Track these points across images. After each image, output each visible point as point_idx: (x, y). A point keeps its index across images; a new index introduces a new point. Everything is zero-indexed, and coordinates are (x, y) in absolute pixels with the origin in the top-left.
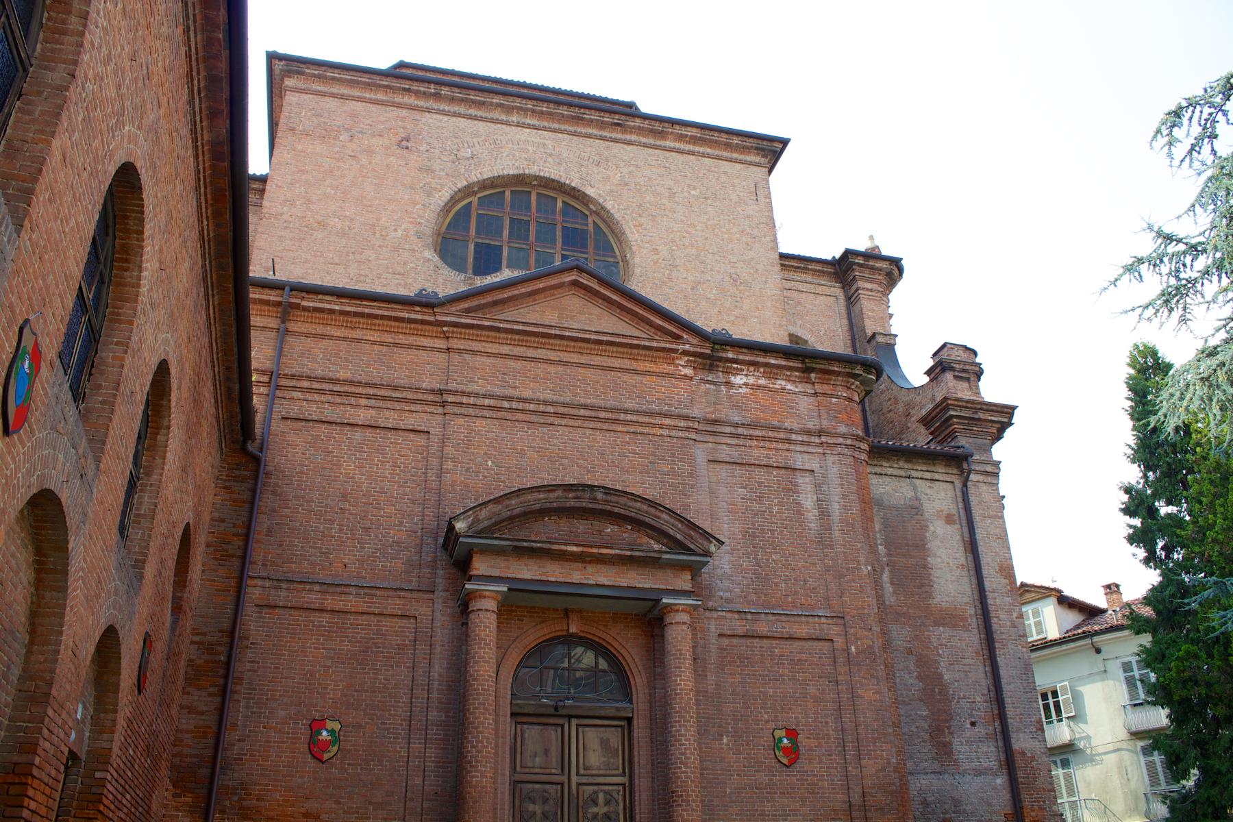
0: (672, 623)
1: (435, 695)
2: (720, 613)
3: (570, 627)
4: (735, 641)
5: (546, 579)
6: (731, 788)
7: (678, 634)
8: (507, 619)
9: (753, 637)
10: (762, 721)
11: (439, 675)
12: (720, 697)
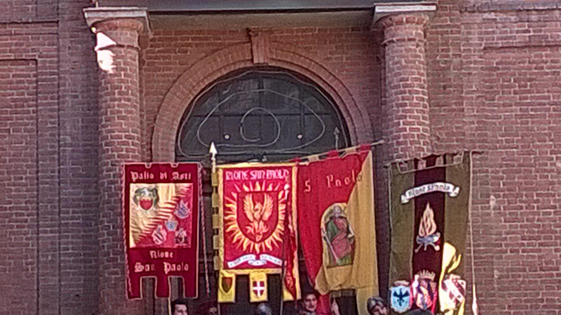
2: (486, 15)
3: (255, 54)
4: (511, 55)
9: (540, 47)
10: (552, 171)
12: (485, 141)
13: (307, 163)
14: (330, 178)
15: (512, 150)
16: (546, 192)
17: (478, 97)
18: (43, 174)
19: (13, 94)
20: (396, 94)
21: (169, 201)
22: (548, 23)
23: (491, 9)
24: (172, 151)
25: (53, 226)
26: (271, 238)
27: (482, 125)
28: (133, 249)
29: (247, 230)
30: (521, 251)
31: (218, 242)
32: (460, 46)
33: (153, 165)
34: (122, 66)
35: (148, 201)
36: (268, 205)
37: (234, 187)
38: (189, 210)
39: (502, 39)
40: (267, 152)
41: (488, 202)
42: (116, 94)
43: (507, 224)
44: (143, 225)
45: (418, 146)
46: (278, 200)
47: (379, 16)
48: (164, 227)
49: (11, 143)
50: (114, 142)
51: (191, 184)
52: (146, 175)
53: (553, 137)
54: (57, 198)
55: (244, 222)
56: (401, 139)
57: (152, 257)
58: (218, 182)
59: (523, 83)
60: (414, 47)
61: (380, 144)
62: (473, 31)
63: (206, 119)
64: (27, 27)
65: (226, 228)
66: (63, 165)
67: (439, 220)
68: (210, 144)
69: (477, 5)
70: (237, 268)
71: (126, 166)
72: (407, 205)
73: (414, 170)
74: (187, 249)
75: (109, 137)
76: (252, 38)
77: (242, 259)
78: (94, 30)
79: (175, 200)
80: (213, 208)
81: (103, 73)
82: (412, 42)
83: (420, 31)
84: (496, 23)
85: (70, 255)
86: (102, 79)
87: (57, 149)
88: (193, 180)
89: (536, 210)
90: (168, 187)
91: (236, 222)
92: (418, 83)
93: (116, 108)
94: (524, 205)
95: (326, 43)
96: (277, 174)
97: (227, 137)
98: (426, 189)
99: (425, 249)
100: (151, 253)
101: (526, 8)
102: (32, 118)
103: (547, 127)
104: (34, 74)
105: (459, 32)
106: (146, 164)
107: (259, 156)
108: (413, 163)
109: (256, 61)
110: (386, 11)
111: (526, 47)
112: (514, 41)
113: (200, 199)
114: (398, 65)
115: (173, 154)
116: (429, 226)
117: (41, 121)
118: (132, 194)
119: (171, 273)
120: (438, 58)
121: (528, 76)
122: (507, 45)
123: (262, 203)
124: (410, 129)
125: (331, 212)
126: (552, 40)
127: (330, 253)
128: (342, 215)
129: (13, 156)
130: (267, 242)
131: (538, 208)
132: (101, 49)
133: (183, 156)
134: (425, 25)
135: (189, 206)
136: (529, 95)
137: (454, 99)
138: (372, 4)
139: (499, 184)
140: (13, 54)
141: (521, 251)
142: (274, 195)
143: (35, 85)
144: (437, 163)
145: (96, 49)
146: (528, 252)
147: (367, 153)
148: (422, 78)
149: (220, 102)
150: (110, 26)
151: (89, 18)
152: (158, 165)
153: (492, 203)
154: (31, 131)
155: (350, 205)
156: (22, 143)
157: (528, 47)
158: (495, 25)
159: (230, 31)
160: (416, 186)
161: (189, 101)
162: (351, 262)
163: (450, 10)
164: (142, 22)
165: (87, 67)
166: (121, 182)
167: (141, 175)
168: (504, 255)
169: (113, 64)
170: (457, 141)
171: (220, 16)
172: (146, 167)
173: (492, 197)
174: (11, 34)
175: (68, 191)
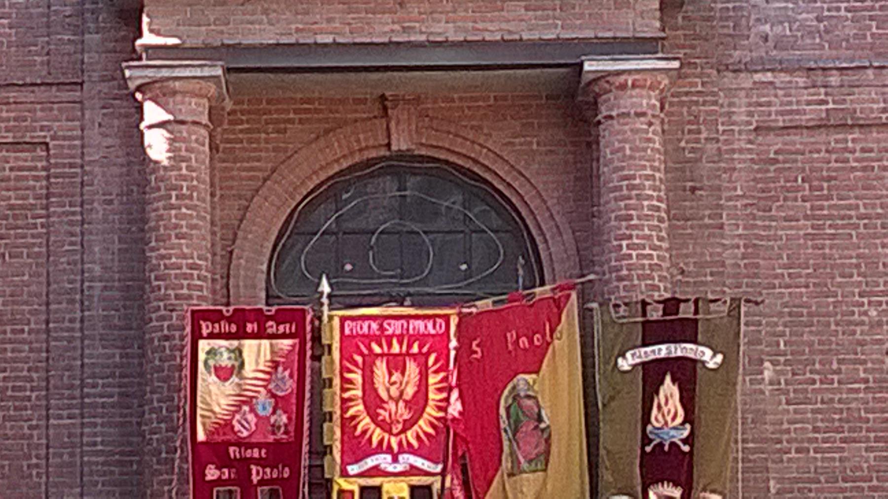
0: (611, 117)
1: (97, 312)
2: (758, 77)
3: (394, 137)
4: (798, 140)
5: (310, 41)
6: (779, 480)
7: (625, 141)
8: (247, 131)
9: (843, 126)
10: (862, 323)
11: (105, 268)
12: (756, 275)
13: (474, 310)
14: (512, 336)
15: (798, 290)
16: (853, 356)
17: (746, 206)
18: (56, 325)
19: (9, 198)
20: (616, 199)
21: (262, 367)
22: (856, 90)
23: (767, 67)
24: (261, 290)
25: (70, 407)
26: (416, 427)
27: (752, 248)
28: (202, 443)
29: (378, 415)
30: (812, 451)
31: (333, 433)
32: (717, 125)
33: (235, 310)
34: (183, 153)
35: (226, 367)
36: (412, 376)
37: (358, 347)
38: (291, 381)
39: (782, 113)
40: (412, 290)
41: (762, 373)
42: (174, 198)
43: (791, 408)
44: (219, 405)
45: (649, 282)
46: (427, 368)
47: (591, 76)
48: (252, 410)
49: (7, 276)
50: (170, 275)
51: (297, 341)
52: (225, 327)
53: (863, 269)
54: (79, 363)
55: (373, 402)
56: (625, 272)
57: (232, 456)
58: (332, 338)
59: (816, 183)
60: (645, 127)
61: (590, 281)
62: (736, 100)
63: (317, 237)
64: (33, 92)
65: (344, 410)
66: (89, 310)
67: (687, 401)
68: (320, 279)
69: (744, 61)
70: (361, 475)
71: (193, 312)
72: (627, 375)
73: (640, 319)
74: (289, 443)
75: (162, 267)
76: (390, 111)
77: (370, 462)
78: (139, 96)
79: (269, 367)
80: (324, 380)
81: (152, 165)
82: (642, 119)
83: (654, 101)
84: (775, 88)
85: (97, 453)
86: (151, 174)
87: (78, 285)
88: (299, 334)
89: (836, 385)
90: (259, 346)
91: (360, 401)
92: (650, 183)
93: (174, 220)
94: (817, 377)
95: (505, 119)
96: (426, 327)
97: (348, 267)
98: (663, 351)
99: (666, 448)
100: (231, 449)
101: (821, 65)
102: (39, 236)
103: (854, 254)
104: (43, 167)
105: (715, 103)
106: (224, 309)
107: (398, 297)
108: (639, 306)
109: (394, 148)
110: (600, 68)
111: (819, 127)
112: (804, 117)
113: (308, 363)
114: (620, 155)
115: (263, 295)
116: (673, 411)
117: (55, 242)
118: (202, 356)
119: (262, 482)
120: (683, 144)
121: (825, 173)
122: (794, 124)
123: (403, 373)
124: (637, 256)
125: (514, 388)
126: (863, 116)
127: (512, 454)
128: (531, 393)
129: (11, 296)
130: (410, 435)
131: (839, 382)
132: (150, 127)
133: (279, 297)
134: (662, 91)
135: (291, 376)
136: (826, 203)
137: (707, 208)
138: (579, 57)
139: (778, 345)
140: (11, 135)
141: (812, 451)
142: (421, 359)
143: (44, 183)
144: (681, 310)
145: (142, 126)
146: (823, 452)
147: (568, 296)
148: (657, 175)
149: (337, 212)
150: (165, 90)
151: (130, 78)
152: (244, 310)
153: (767, 374)
154: (38, 254)
155: (543, 379)
156: (24, 275)
157: (825, 126)
158: (773, 92)
159: (354, 100)
160: (645, 345)
161: (289, 211)
162: (544, 467)
163: (702, 68)
164: (215, 84)
165: (128, 154)
166: (182, 338)
167: (217, 325)
168: (785, 457)
169: (169, 151)
170: (712, 274)
171: (337, 76)
172: (224, 312)
173: (767, 364)
174: (8, 103)
175: (96, 353)
